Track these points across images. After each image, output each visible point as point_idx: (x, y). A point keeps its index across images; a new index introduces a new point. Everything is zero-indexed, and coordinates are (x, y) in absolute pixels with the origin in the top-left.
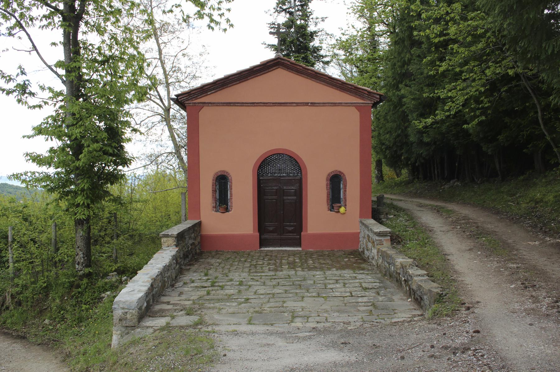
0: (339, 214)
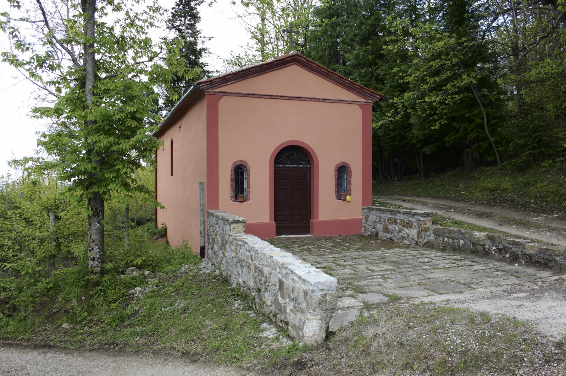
0: (345, 202)
